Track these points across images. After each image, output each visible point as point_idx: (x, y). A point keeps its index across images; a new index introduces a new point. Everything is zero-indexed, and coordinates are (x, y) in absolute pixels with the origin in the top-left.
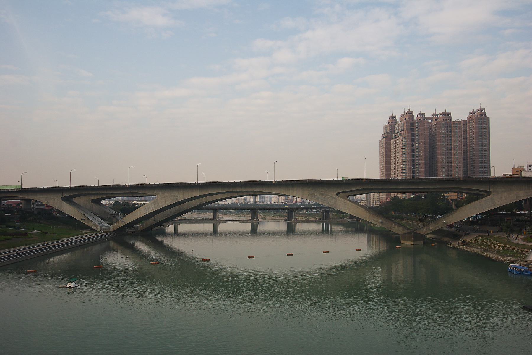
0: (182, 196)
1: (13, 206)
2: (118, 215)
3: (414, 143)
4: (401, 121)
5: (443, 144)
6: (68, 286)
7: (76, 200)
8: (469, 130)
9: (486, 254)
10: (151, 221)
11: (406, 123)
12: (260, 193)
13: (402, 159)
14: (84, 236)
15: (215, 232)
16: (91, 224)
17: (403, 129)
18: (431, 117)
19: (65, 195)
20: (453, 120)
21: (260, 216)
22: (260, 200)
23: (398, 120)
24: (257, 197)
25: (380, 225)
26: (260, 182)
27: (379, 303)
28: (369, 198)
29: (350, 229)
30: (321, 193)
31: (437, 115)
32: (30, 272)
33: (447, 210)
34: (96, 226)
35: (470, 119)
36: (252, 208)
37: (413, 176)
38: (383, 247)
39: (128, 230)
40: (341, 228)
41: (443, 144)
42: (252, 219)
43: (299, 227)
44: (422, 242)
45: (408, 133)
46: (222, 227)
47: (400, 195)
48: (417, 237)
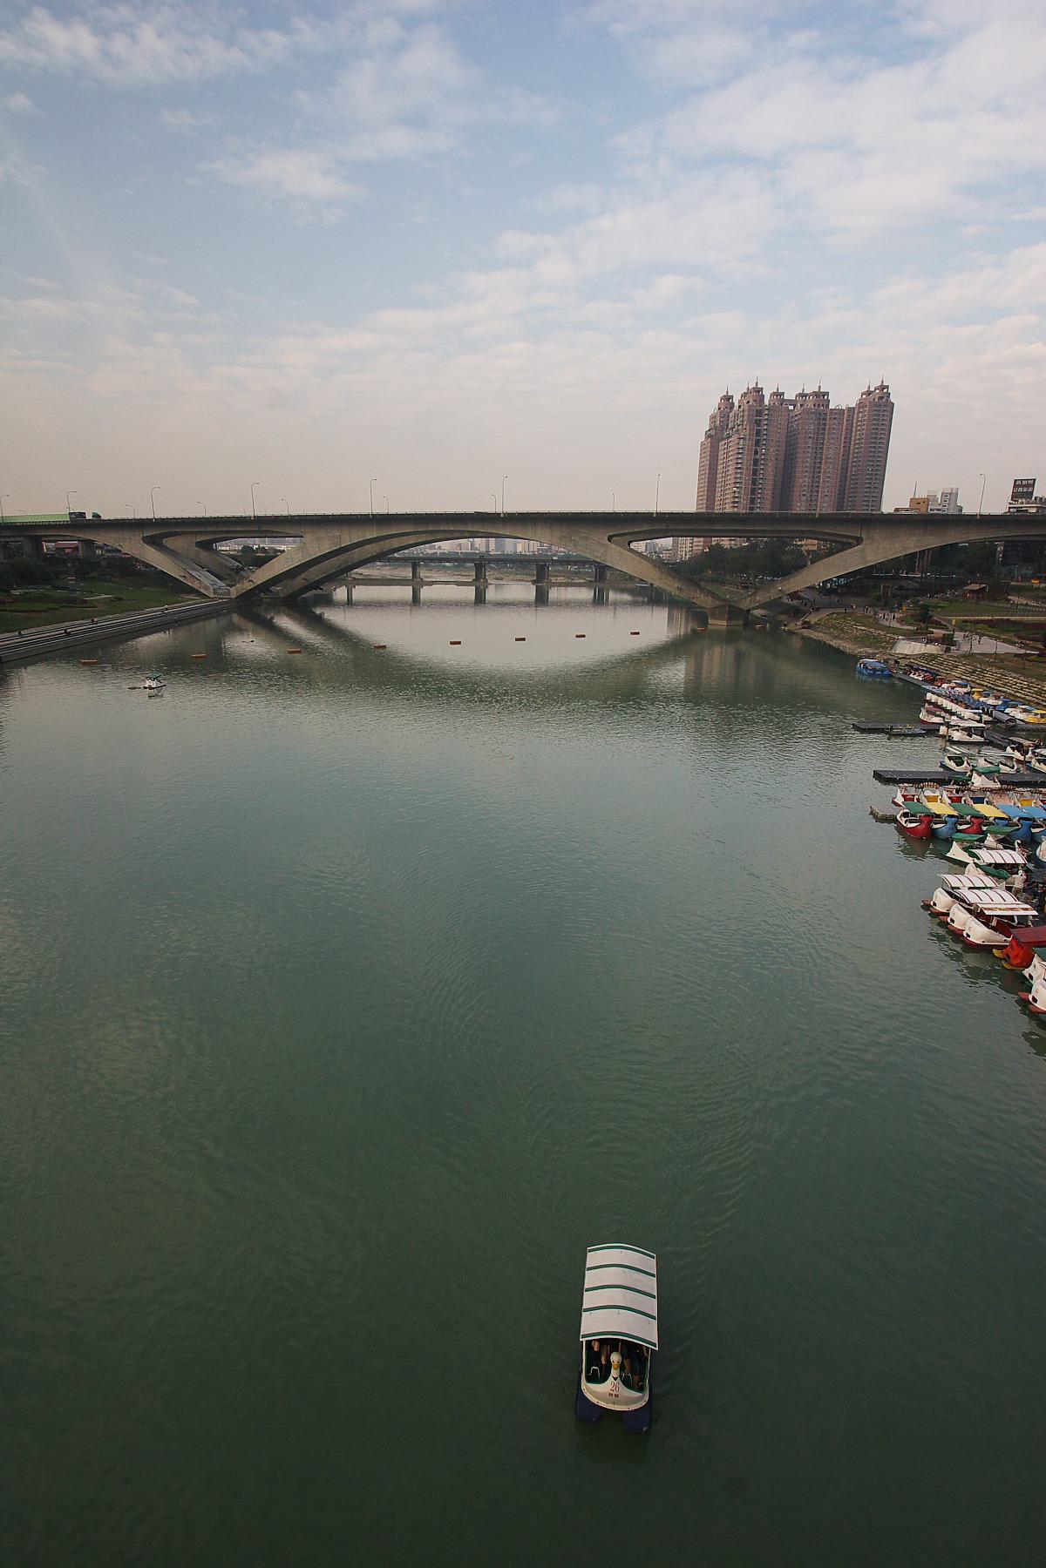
0: (348, 537)
1: (67, 551)
2: (243, 569)
4: (740, 407)
6: (147, 686)
7: (167, 542)
8: (857, 426)
9: (834, 643)
10: (300, 581)
11: (750, 410)
12: (480, 535)
13: (736, 478)
14: (189, 604)
15: (416, 600)
16: (199, 585)
17: (742, 421)
20: (831, 406)
21: (490, 575)
22: (498, 548)
23: (736, 404)
24: (492, 540)
25: (677, 592)
26: (293, 517)
27: (284, 711)
29: (640, 599)
30: (582, 535)
31: (806, 395)
32: (85, 664)
33: (798, 565)
34: (207, 588)
35: (861, 404)
36: (476, 560)
37: (752, 509)
38: (682, 628)
39: (262, 595)
40: (627, 597)
42: (477, 578)
43: (554, 594)
44: (741, 622)
46: (426, 593)
47: (726, 543)
48: (733, 613)
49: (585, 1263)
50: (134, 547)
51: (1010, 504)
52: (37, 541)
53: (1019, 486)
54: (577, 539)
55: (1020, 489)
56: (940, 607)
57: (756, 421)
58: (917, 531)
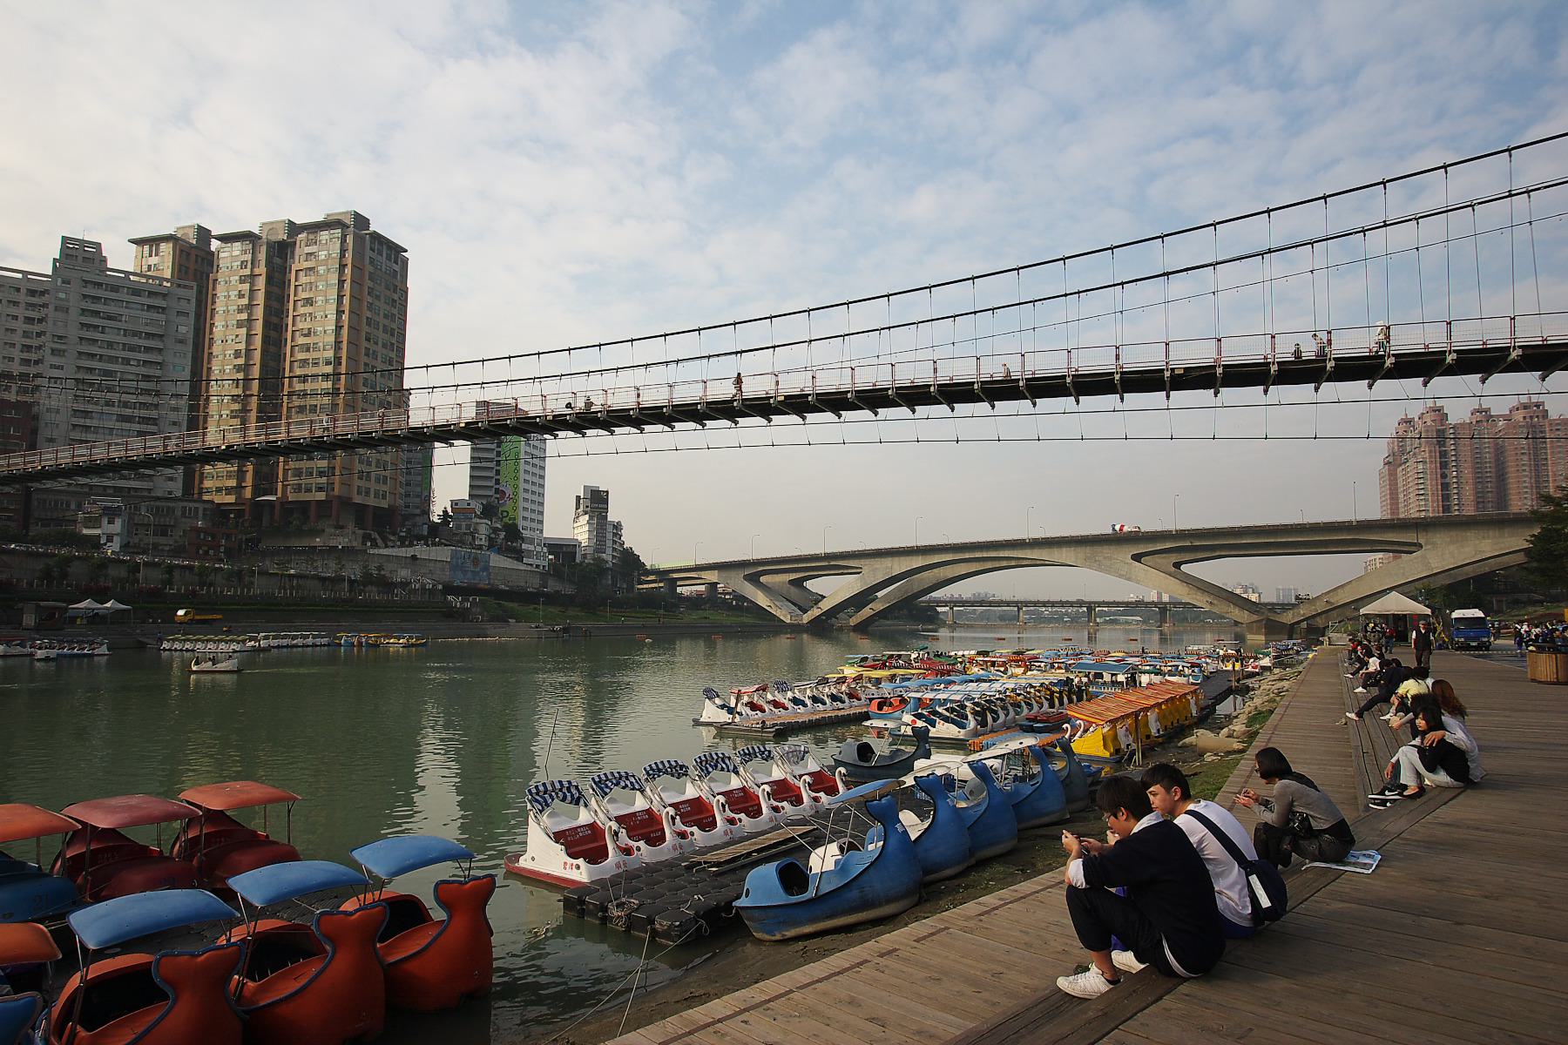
5: (1524, 470)
18: (1508, 413)
19: (748, 572)
41: (1524, 470)
45: (1430, 452)
49: (403, 357)
52: (673, 583)
54: (1101, 558)
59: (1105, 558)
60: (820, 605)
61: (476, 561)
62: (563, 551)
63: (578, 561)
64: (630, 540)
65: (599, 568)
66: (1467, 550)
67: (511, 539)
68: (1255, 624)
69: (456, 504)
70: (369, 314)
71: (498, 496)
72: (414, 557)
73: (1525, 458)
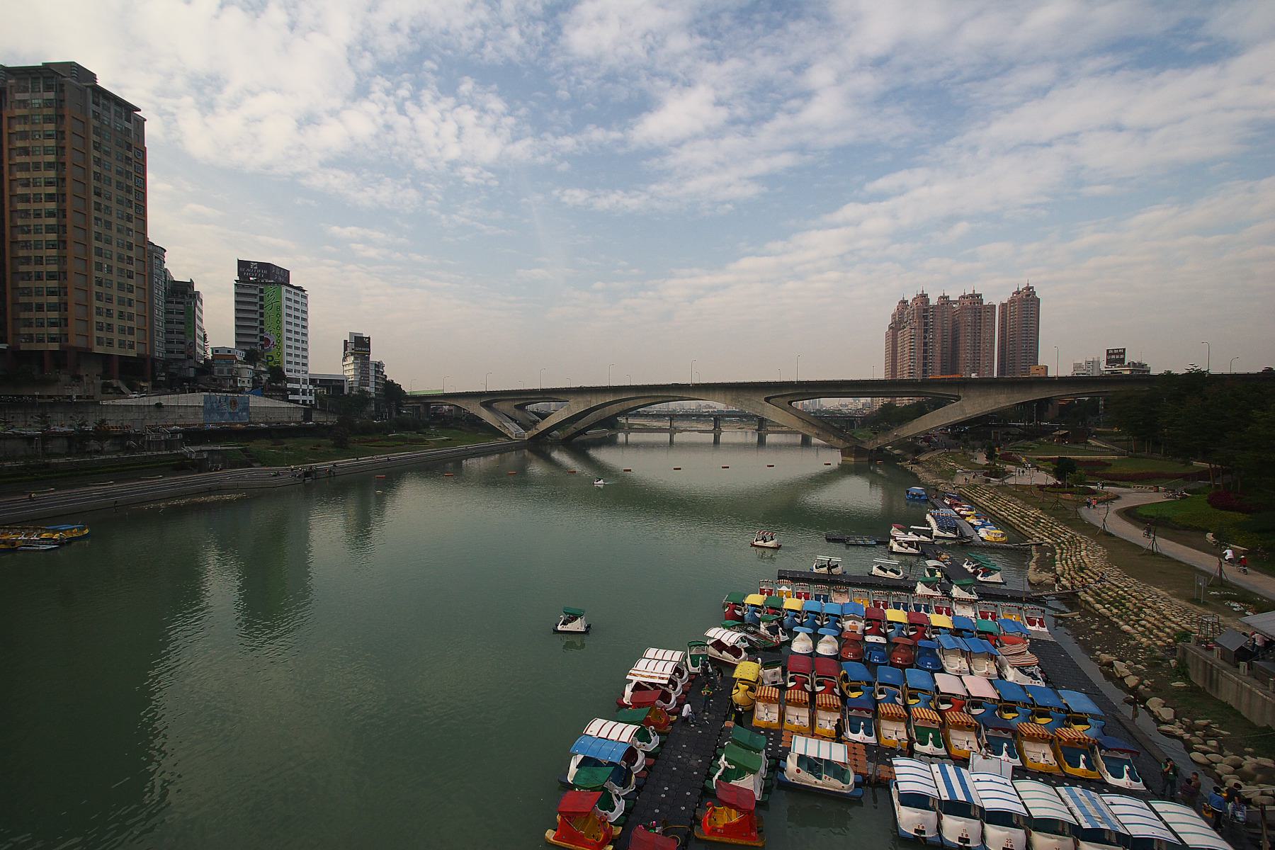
3: (927, 335)
10: (571, 429)
11: (918, 309)
28: (872, 401)
34: (512, 434)
35: (1012, 301)
44: (868, 459)
50: (476, 409)
51: (1106, 368)
53: (1111, 354)
54: (743, 400)
55: (1113, 357)
56: (1031, 448)
57: (924, 316)
58: (1006, 390)
59: (746, 400)
60: (538, 426)
61: (234, 403)
62: (332, 386)
63: (346, 393)
64: (391, 374)
65: (363, 398)
66: (990, 401)
67: (275, 382)
68: (847, 450)
69: (217, 351)
70: (97, 169)
71: (263, 343)
72: (159, 406)
73: (969, 328)
